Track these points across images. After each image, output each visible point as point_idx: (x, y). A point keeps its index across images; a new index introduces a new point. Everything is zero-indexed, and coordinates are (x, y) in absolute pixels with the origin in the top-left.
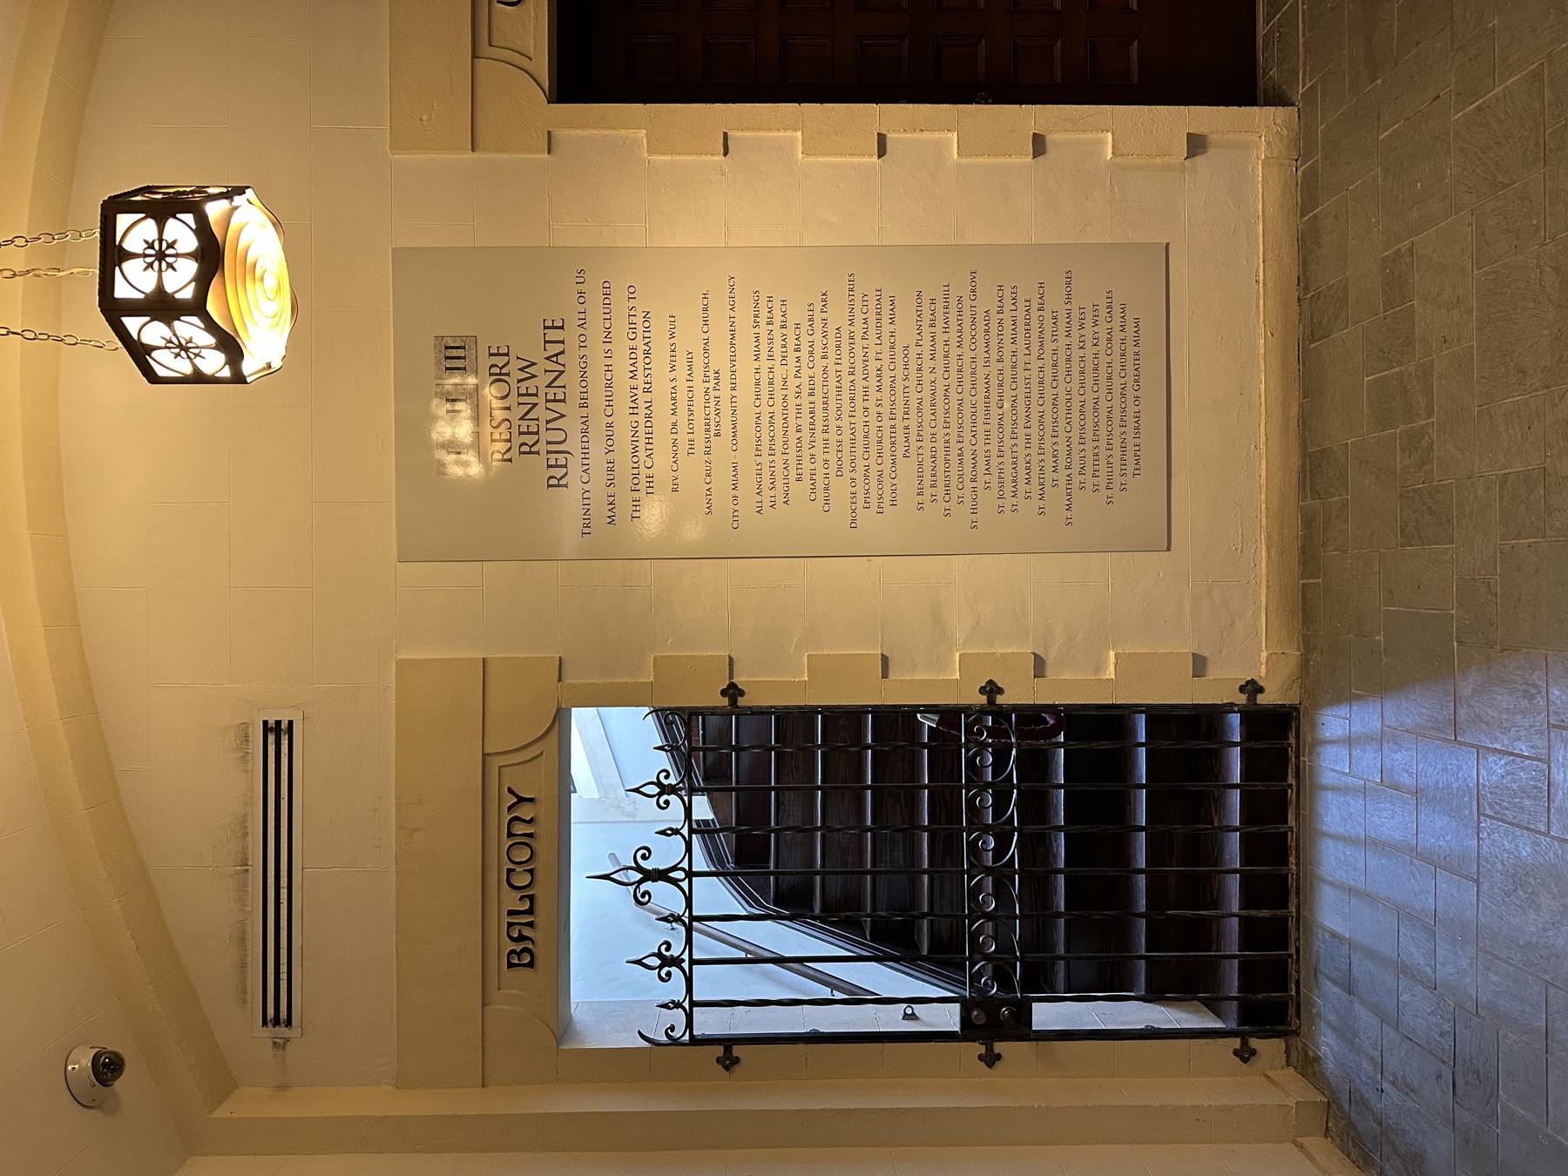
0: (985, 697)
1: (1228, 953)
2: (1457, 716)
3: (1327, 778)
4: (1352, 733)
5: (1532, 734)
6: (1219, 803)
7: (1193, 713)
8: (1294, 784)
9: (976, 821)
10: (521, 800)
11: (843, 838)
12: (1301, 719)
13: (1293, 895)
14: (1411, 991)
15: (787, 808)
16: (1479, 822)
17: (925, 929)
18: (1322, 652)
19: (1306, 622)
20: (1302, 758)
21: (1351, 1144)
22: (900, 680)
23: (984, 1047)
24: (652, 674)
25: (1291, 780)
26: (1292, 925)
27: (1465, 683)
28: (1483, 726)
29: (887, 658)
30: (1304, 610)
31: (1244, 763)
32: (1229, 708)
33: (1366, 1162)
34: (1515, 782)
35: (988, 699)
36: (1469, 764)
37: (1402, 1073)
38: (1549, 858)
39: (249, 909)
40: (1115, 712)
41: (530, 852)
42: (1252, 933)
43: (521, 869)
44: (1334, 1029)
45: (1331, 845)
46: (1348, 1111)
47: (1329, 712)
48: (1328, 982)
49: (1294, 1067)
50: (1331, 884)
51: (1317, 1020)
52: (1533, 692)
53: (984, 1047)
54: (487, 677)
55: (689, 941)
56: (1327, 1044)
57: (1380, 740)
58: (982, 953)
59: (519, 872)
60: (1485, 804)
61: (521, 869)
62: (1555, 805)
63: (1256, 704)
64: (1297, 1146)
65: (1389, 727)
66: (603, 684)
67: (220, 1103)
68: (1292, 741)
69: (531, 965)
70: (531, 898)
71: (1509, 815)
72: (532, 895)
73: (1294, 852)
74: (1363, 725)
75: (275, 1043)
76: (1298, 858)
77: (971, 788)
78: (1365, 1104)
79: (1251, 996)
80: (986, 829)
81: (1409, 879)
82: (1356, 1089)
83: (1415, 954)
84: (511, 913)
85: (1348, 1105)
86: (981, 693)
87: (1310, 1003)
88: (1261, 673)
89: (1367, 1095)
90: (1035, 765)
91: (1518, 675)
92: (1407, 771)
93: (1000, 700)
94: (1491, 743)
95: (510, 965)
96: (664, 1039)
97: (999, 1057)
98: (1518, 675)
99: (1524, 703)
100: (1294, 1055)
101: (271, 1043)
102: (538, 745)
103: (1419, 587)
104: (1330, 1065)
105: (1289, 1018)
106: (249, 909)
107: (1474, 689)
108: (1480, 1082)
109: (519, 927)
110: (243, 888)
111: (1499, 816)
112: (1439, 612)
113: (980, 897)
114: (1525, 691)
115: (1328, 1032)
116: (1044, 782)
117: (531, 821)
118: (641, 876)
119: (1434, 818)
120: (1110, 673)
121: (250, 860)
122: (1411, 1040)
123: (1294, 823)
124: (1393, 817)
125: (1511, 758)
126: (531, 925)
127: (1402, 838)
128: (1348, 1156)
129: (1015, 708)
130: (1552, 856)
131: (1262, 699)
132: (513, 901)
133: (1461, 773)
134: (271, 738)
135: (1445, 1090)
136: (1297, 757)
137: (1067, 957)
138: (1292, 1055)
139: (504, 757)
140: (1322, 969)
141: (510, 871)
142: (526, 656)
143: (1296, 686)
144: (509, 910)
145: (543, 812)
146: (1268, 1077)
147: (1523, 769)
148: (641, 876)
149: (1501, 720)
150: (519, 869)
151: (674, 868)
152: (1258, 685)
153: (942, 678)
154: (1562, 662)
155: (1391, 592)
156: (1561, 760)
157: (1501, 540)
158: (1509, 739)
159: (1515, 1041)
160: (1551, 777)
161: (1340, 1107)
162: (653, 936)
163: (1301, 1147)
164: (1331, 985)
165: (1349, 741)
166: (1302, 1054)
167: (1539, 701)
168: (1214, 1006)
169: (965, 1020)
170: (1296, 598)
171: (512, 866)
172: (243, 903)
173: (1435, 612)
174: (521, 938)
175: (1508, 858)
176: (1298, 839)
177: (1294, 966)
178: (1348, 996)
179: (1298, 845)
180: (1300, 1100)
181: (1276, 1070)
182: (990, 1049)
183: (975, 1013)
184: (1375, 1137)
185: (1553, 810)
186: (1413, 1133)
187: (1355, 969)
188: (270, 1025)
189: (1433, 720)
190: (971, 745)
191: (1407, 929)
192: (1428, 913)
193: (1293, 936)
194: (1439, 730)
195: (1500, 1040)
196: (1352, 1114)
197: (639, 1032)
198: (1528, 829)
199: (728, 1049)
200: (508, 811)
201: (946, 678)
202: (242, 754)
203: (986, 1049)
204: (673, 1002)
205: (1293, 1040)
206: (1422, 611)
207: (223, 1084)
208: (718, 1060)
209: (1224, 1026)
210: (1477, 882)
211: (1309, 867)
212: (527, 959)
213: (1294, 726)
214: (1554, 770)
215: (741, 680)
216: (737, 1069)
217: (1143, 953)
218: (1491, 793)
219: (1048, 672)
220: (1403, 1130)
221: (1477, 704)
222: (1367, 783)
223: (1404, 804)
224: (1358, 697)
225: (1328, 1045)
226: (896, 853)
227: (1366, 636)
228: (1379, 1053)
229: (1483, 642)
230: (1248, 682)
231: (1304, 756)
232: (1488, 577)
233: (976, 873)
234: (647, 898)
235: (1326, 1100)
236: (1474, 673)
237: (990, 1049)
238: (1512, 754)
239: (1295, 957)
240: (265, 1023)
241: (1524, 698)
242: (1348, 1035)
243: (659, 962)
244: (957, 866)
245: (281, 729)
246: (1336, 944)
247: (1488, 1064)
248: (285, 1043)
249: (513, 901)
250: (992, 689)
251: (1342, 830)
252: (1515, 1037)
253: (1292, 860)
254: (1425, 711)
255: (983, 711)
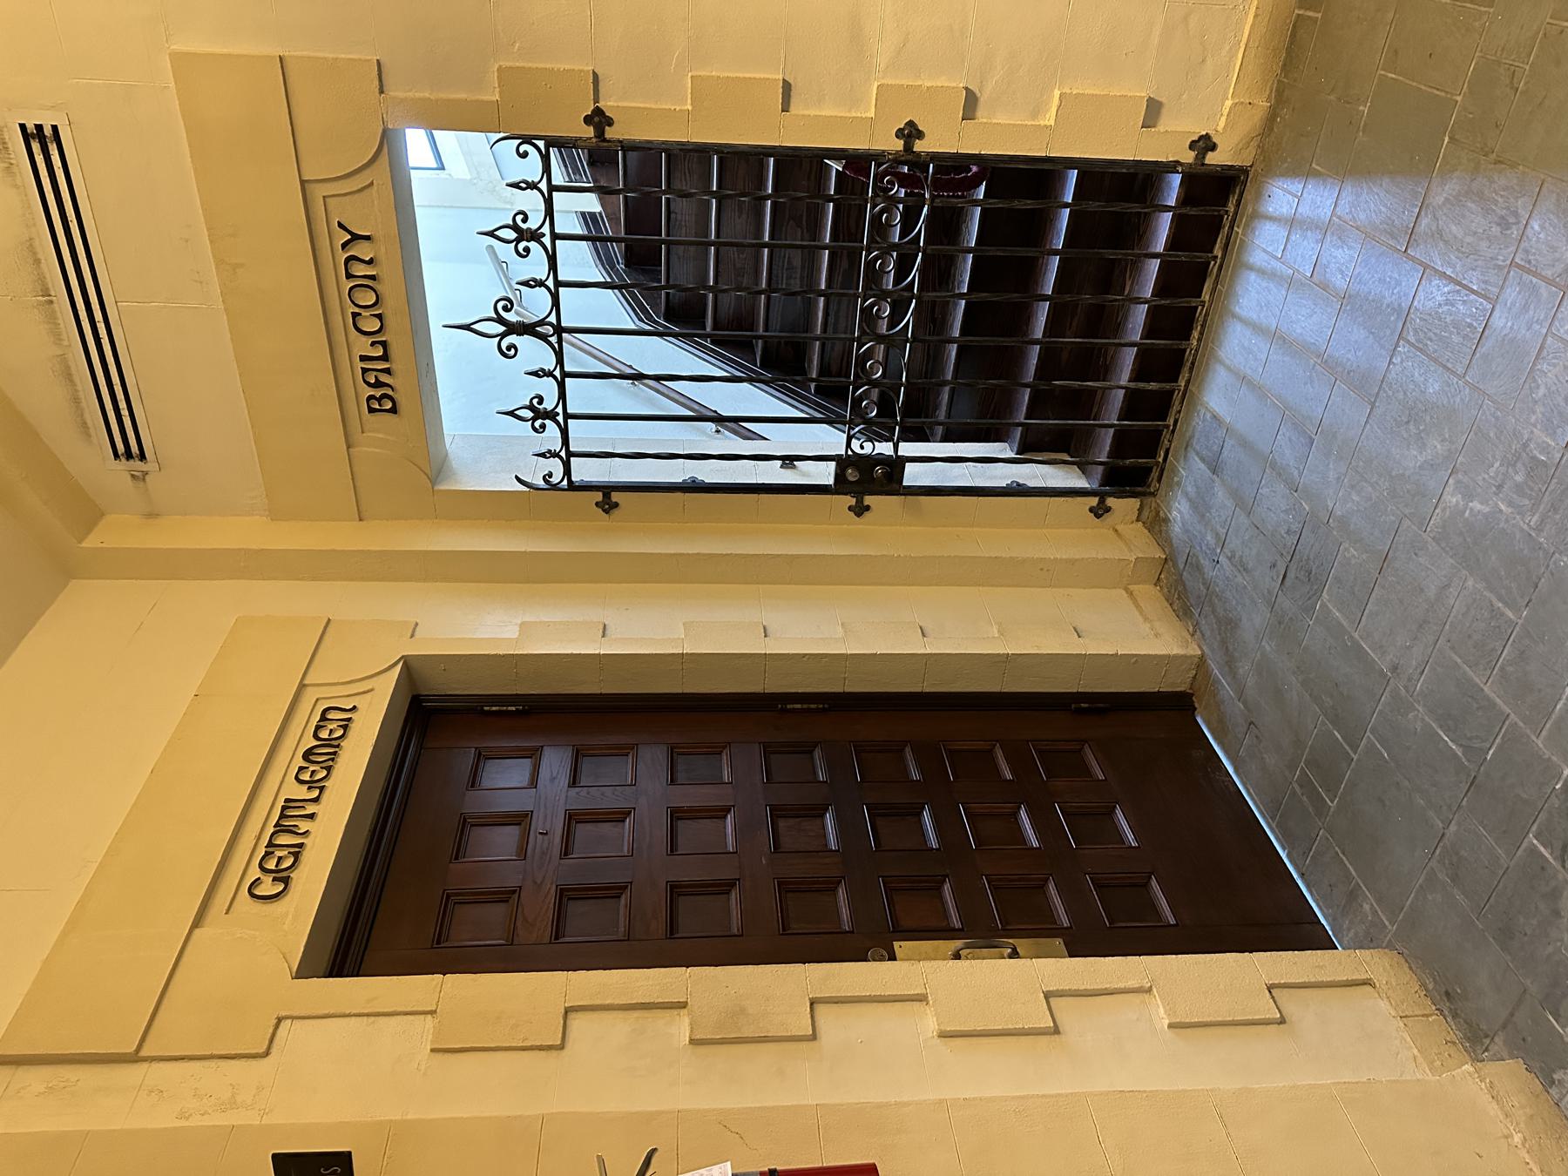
0: (902, 142)
1: (1106, 422)
2: (1417, 226)
3: (1256, 257)
4: (1297, 215)
5: (1489, 268)
6: (1136, 266)
7: (1132, 171)
8: (1219, 256)
9: (874, 287)
10: (355, 237)
11: (739, 258)
12: (1248, 184)
13: (1186, 369)
14: (1272, 486)
15: (679, 217)
16: (1397, 345)
17: (815, 363)
18: (1293, 109)
19: (1286, 67)
20: (1235, 228)
21: (1176, 596)
22: (803, 115)
23: (855, 500)
24: (498, 90)
25: (1218, 251)
26: (1177, 397)
27: (1440, 189)
28: (1441, 244)
29: (790, 85)
30: (1289, 51)
31: (1173, 230)
32: (1172, 167)
33: (1185, 614)
34: (1451, 315)
35: (905, 145)
36: (1411, 280)
37: (1241, 553)
38: (1454, 402)
39: (66, 343)
40: (1046, 166)
41: (375, 296)
42: (1135, 404)
43: (368, 314)
44: (1190, 500)
45: (1239, 329)
46: (1182, 567)
47: (1280, 184)
48: (1196, 458)
49: (1144, 523)
50: (1228, 368)
51: (1176, 488)
52: (1511, 221)
53: (855, 500)
54: (290, 81)
55: (562, 395)
56: (1179, 511)
57: (1324, 229)
58: (863, 418)
59: (366, 317)
60: (1410, 329)
61: (368, 314)
62: (1482, 350)
63: (1203, 164)
64: (1127, 592)
65: (1339, 218)
66: (437, 100)
67: (89, 530)
68: (1231, 208)
69: (394, 410)
70: (384, 344)
71: (1431, 346)
72: (385, 342)
73: (1199, 328)
74: (1312, 208)
75: (132, 475)
76: (1201, 333)
77: (871, 250)
78: (1198, 568)
79: (1119, 461)
80: (883, 295)
81: (1306, 384)
82: (1194, 555)
83: (1287, 454)
84: (363, 358)
85: (1183, 565)
86: (897, 136)
87: (1174, 471)
88: (1217, 126)
89: (1202, 561)
90: (946, 225)
91: (1502, 196)
92: (1342, 272)
93: (919, 146)
94: (1442, 266)
95: (371, 410)
96: (541, 483)
97: (868, 508)
98: (1502, 196)
99: (1496, 230)
100: (1146, 513)
101: (129, 477)
102: (367, 172)
103: (1431, 55)
104: (1176, 529)
105: (1150, 479)
106: (66, 343)
107: (1447, 199)
108: (1309, 580)
109: (375, 373)
110: (52, 318)
111: (1421, 346)
112: (1443, 94)
113: (868, 364)
114: (1502, 217)
115: (1184, 501)
116: (953, 245)
117: (371, 262)
118: (504, 328)
119: (1352, 330)
120: (1049, 119)
121: (51, 289)
122: (1258, 528)
123: (1207, 297)
124: (1311, 316)
125: (1458, 288)
126: (388, 371)
127: (1313, 341)
128: (1171, 604)
129: (934, 157)
130: (1458, 400)
131: (1212, 158)
132: (363, 346)
133: (1398, 289)
134: (36, 146)
135: (1275, 578)
136: (1231, 228)
137: (946, 423)
138: (1144, 512)
139: (328, 185)
140: (1194, 444)
141: (355, 315)
142: (334, 56)
143: (1254, 144)
144: (360, 356)
145: (384, 250)
146: (1116, 531)
147: (1464, 302)
148: (504, 328)
149: (1462, 241)
150: (365, 313)
151: (542, 322)
152: (1211, 141)
153: (854, 115)
154: (1558, 194)
155: (1396, 52)
156: (1508, 305)
157: (1551, 18)
158: (1463, 266)
159: (1354, 555)
160: (1491, 319)
161: (1175, 565)
162: (525, 391)
163: (1131, 594)
164: (1199, 461)
165: (1292, 223)
166: (1154, 513)
167: (1512, 233)
168: (1083, 467)
169: (839, 476)
170: (1285, 32)
171: (357, 310)
172: (57, 337)
173: (1438, 93)
174: (378, 384)
175: (1414, 390)
176: (1207, 315)
177: (1168, 436)
178: (1211, 474)
179: (1205, 321)
180: (1140, 556)
181: (1126, 524)
182: (860, 502)
183: (850, 471)
184: (1199, 597)
185: (1478, 355)
186: (1234, 603)
187: (1225, 452)
188: (123, 459)
189: (1390, 222)
190: (879, 200)
191: (1287, 430)
192: (1314, 421)
193: (1175, 408)
194: (1391, 235)
195: (1340, 551)
196: (1185, 573)
197: (517, 477)
198: (1445, 367)
199: (608, 496)
200: (343, 249)
201: (859, 115)
202: (6, 165)
203: (856, 502)
204: (549, 451)
205: (1149, 499)
206: (1423, 87)
207: (88, 514)
208: (597, 504)
209: (1087, 486)
210: (1373, 405)
211: (1210, 344)
212: (389, 405)
213: (1237, 191)
214: (1496, 314)
215: (609, 103)
216: (615, 512)
217: (1023, 421)
218: (1420, 319)
219: (980, 112)
220: (1225, 598)
221: (1444, 218)
222: (1296, 273)
223: (1327, 306)
224: (1317, 174)
225: (1180, 512)
226: (792, 281)
227: (1348, 103)
228: (1225, 531)
229: (1478, 145)
230: (1201, 137)
231: (1238, 227)
232: (1516, 64)
233: (866, 341)
234: (513, 351)
235: (1164, 557)
236: (1454, 181)
237: (860, 502)
238: (1459, 284)
239: (1171, 428)
240: (116, 455)
241: (1499, 224)
242: (1200, 507)
243: (532, 415)
244: (845, 333)
245: (45, 137)
246: (1215, 425)
247: (1322, 568)
248: (144, 476)
249: (363, 346)
250: (911, 133)
251: (1255, 317)
252: (1355, 553)
253: (1195, 334)
254: (1383, 209)
255: (897, 160)
